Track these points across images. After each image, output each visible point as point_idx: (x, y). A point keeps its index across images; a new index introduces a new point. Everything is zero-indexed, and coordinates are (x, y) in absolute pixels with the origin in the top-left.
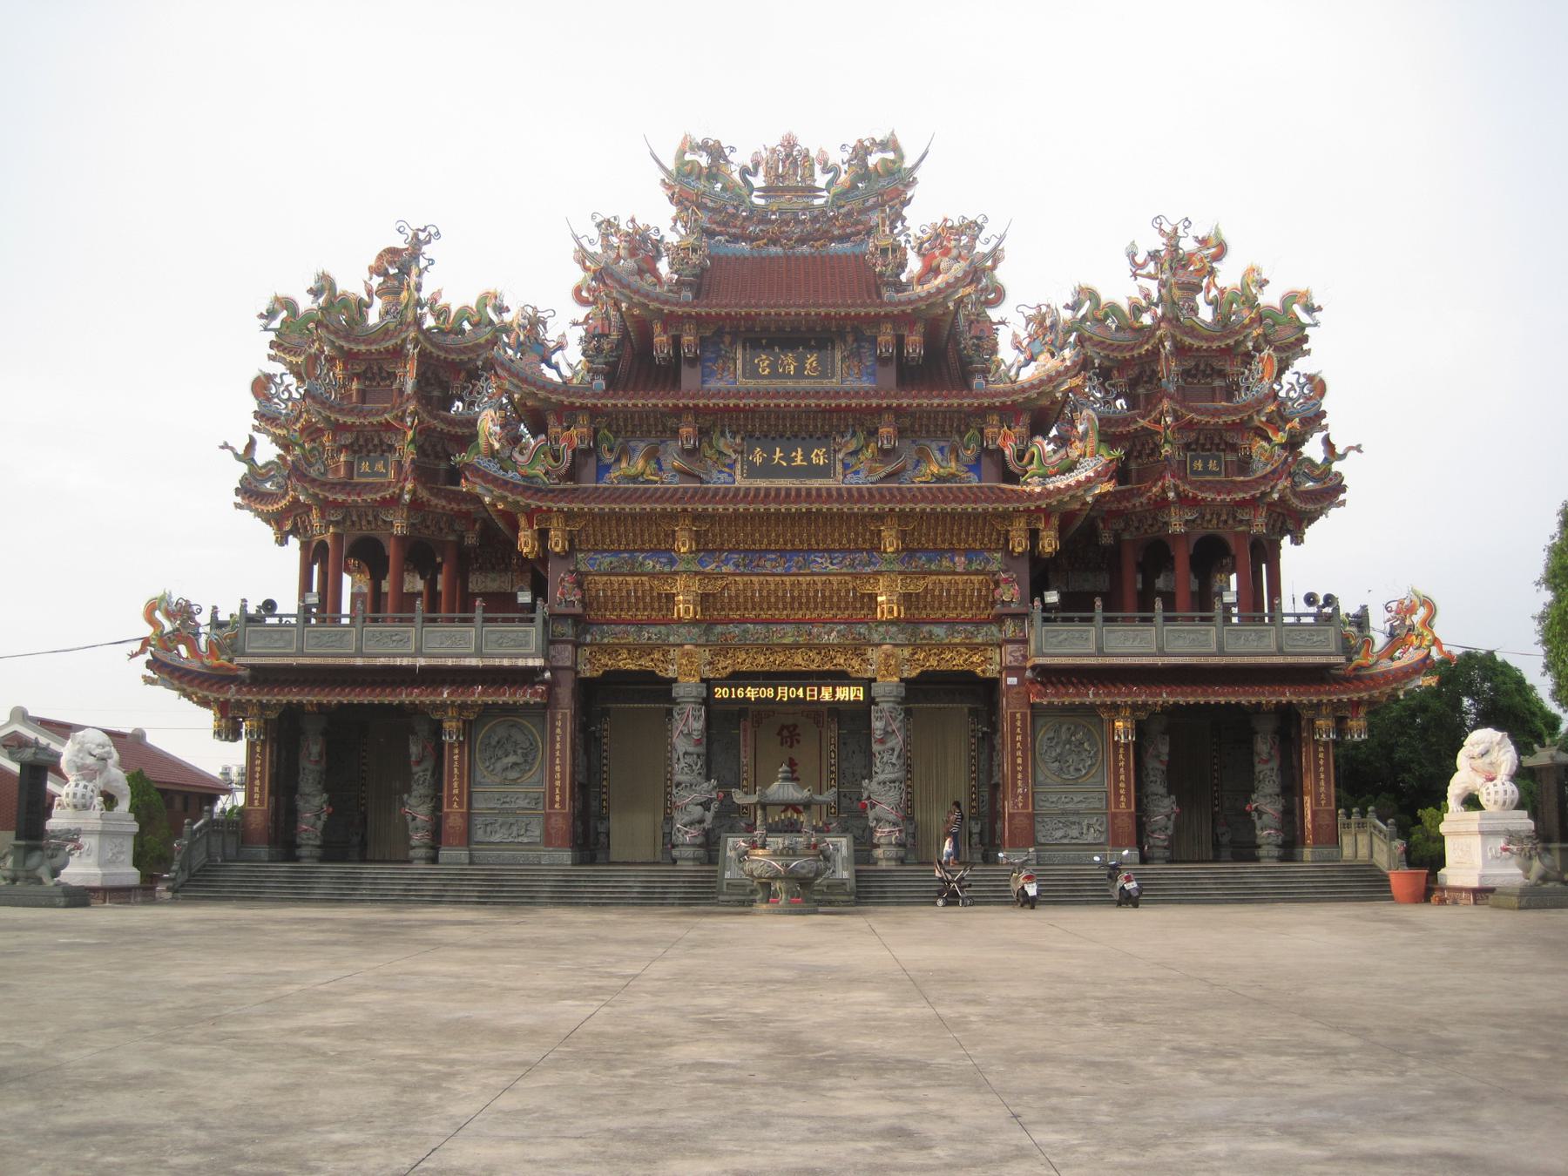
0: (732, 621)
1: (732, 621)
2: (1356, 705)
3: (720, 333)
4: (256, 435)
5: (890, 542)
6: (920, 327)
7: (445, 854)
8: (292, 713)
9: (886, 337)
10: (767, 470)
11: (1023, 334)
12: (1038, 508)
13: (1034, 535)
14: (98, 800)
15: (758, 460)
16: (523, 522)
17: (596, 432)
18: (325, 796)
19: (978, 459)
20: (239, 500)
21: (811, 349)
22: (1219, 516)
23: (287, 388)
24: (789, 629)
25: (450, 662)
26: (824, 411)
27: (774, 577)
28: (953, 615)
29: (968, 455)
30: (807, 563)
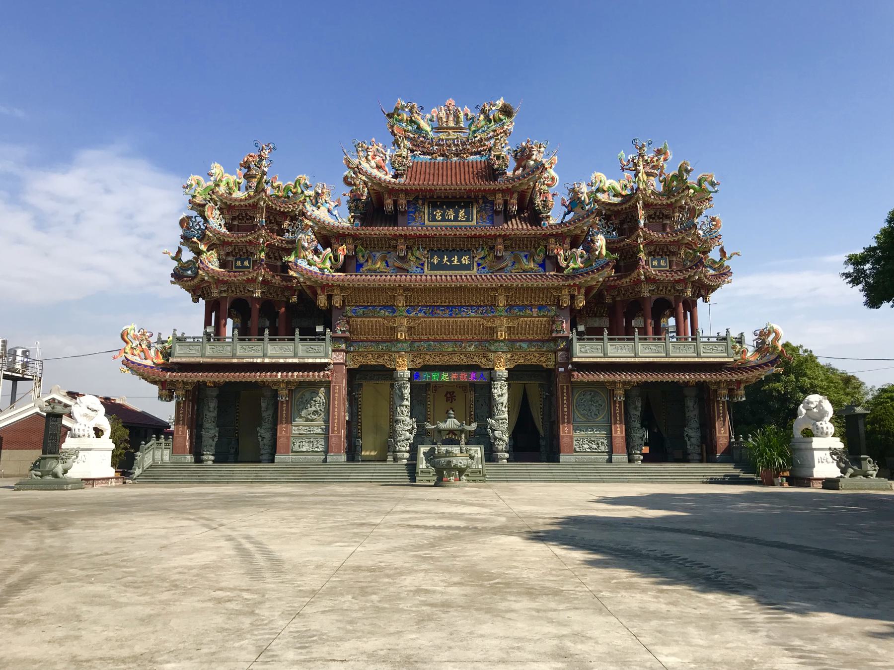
0: (423, 340)
1: (423, 340)
2: (739, 383)
3: (417, 199)
4: (182, 247)
5: (502, 302)
6: (515, 196)
7: (277, 458)
8: (200, 386)
9: (499, 199)
10: (440, 267)
11: (567, 198)
12: (575, 284)
13: (572, 297)
14: (92, 433)
15: (436, 262)
16: (319, 291)
17: (356, 247)
18: (217, 429)
19: (544, 261)
20: (173, 279)
21: (461, 208)
22: (666, 288)
23: (198, 224)
24: (450, 344)
25: (282, 361)
26: (468, 237)
27: (442, 320)
28: (530, 337)
29: (539, 259)
30: (460, 312)
